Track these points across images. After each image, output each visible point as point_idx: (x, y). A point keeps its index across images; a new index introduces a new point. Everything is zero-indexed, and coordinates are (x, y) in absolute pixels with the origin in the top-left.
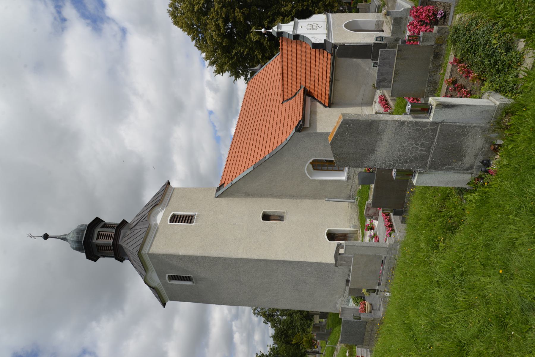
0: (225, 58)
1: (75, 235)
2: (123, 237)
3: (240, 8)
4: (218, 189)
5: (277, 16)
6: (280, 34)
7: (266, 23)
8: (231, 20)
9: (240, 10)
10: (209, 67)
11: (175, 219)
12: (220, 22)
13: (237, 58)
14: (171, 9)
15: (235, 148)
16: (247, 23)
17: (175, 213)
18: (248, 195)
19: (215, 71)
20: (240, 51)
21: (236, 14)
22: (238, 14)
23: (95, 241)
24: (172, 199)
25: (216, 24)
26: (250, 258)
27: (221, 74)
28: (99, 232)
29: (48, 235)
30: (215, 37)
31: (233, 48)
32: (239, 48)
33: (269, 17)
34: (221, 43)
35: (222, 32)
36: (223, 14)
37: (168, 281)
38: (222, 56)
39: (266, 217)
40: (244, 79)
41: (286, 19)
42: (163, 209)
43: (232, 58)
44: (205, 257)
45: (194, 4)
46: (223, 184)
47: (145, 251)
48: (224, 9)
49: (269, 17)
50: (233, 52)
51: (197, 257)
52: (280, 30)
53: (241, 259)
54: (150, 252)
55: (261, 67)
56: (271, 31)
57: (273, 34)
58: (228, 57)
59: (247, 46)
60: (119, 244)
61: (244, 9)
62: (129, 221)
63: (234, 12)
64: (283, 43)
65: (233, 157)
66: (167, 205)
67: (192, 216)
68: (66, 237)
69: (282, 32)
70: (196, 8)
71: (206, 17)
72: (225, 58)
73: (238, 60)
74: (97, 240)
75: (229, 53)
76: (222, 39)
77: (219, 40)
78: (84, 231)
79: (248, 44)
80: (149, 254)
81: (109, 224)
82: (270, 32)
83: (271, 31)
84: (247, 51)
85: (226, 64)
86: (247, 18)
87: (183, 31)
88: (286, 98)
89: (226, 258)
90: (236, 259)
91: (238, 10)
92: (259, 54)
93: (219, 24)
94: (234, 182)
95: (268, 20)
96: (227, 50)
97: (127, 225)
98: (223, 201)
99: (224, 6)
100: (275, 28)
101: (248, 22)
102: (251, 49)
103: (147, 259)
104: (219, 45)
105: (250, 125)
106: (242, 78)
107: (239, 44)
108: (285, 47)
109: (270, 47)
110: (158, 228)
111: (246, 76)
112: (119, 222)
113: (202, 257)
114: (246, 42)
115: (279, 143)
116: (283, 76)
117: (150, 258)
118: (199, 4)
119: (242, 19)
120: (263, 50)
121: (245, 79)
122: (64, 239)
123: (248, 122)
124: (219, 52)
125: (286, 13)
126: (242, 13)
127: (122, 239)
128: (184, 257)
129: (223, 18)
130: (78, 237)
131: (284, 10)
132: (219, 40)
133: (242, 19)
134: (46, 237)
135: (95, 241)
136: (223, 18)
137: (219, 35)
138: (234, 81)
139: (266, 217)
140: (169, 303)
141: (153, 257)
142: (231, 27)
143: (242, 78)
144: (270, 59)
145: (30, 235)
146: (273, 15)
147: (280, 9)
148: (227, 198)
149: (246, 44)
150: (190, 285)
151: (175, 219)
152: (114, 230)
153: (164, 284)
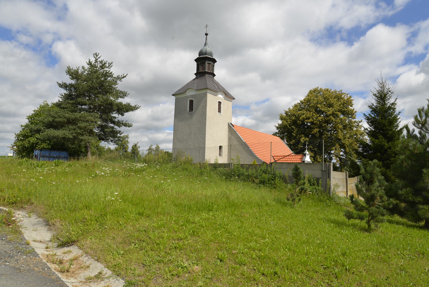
0: (290, 121)
1: (209, 51)
2: (209, 76)
3: (319, 131)
4: (231, 124)
5: (314, 153)
6: (305, 155)
7: (310, 147)
8: (312, 126)
9: (318, 131)
10: (284, 111)
11: (220, 103)
12: (311, 120)
13: (290, 129)
14: (319, 89)
15: (248, 132)
16: (310, 135)
17: (222, 103)
18: (230, 139)
19: (281, 115)
20: (294, 131)
21: (315, 129)
22: (316, 130)
23: (207, 62)
24: (227, 101)
25: (310, 117)
26: (206, 140)
27: (280, 118)
28: (211, 64)
29: (207, 35)
30: (303, 116)
31: (296, 127)
32: (296, 131)
33: (314, 148)
34: (299, 120)
35: (305, 120)
36: (316, 121)
37: (189, 99)
38: (291, 119)
39: (220, 147)
40: (276, 132)
41: (312, 159)
42: (223, 97)
43: (290, 126)
44: (206, 119)
45: (322, 105)
46: (234, 126)
47: (208, 91)
48: (319, 122)
49: (314, 148)
50: (294, 126)
51: (205, 115)
52: (307, 155)
53: (205, 136)
54: (208, 93)
55: (286, 144)
56: (307, 151)
57: (305, 152)
58: (290, 124)
59: (297, 135)
60: (206, 75)
61: (318, 134)
62: (215, 77)
63: (317, 128)
64: (301, 157)
65: (245, 131)
66: (225, 99)
67: (220, 112)
68: (207, 46)
69: (306, 156)
70: (319, 106)
71: (314, 111)
72: (290, 121)
73: (289, 129)
74: (208, 63)
75: (293, 124)
76: (301, 121)
77: (301, 118)
78: (211, 55)
79: (299, 136)
80: (206, 93)
81: (214, 68)
82: (306, 150)
83: (307, 151)
84: (294, 135)
85: (287, 122)
86: (314, 136)
87: (306, 96)
88: (275, 158)
89: (206, 129)
90: (205, 134)
91: (318, 130)
92: (292, 142)
93: (310, 119)
94: (237, 132)
95: (312, 148)
96: (294, 123)
97: (213, 77)
98: (227, 127)
99: (320, 122)
100: (307, 153)
101: (310, 136)
102: (295, 137)
103: (204, 91)
104: (298, 118)
105: (260, 139)
106: (277, 131)
107: (298, 131)
108: (297, 157)
109: (297, 149)
110: (216, 96)
111: (278, 133)
112: (215, 73)
113: (206, 118)
114: (300, 135)
115: (256, 154)
116: (287, 156)
117: (204, 93)
118: (321, 108)
119: (313, 132)
120: (294, 145)
121: (276, 133)
122: (205, 44)
123: (261, 138)
124: (293, 118)
125: (316, 159)
126: (316, 133)
127: (208, 76)
128: (206, 109)
129: (313, 121)
130: (208, 53)
131: (318, 157)
132: (301, 118)
133: (313, 132)
134: (206, 34)
135: (207, 62)
136: (313, 121)
137: (304, 119)
138: (275, 126)
139: (220, 147)
140: (174, 98)
141: (205, 95)
142: (308, 125)
143: (277, 131)
144: (290, 148)
145: (207, 26)
146: (315, 151)
147: (318, 155)
148: (228, 128)
149: (298, 135)
150: (187, 110)
151: (220, 103)
152: (212, 72)
153: (188, 97)
